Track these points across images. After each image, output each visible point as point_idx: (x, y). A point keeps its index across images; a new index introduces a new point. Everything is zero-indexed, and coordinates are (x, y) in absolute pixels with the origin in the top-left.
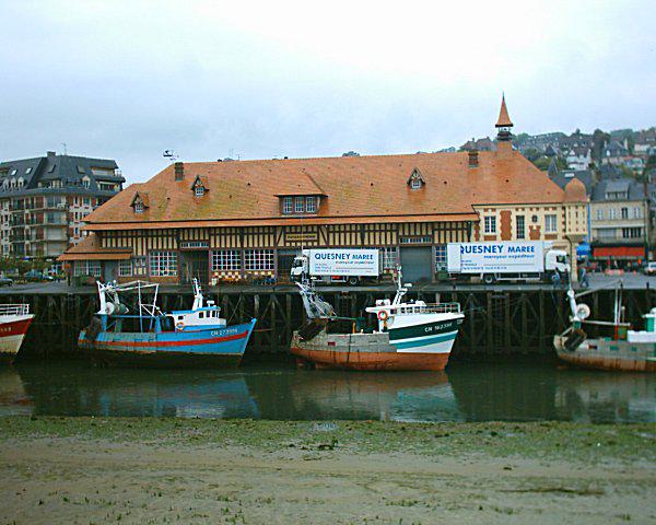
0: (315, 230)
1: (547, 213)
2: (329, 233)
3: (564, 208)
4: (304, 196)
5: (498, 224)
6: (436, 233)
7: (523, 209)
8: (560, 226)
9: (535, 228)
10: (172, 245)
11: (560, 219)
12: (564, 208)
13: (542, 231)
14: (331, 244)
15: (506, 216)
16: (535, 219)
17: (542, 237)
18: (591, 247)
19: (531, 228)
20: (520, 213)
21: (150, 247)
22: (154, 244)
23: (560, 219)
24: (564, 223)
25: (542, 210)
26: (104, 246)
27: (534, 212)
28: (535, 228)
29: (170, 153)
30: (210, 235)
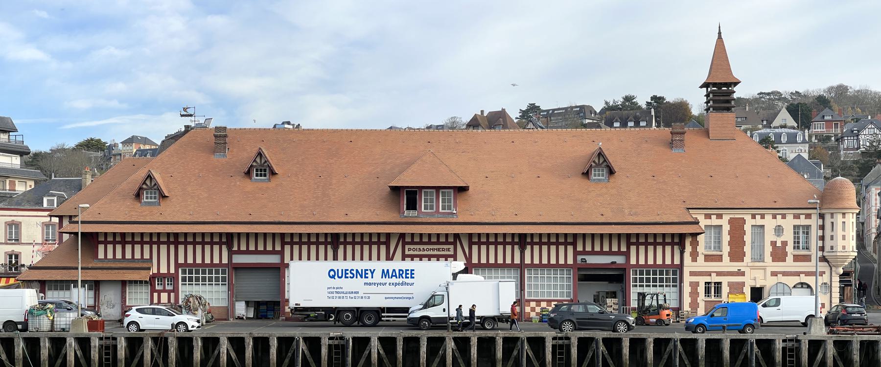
0: (451, 240)
1: (797, 222)
2: (471, 244)
3: (822, 216)
4: (438, 188)
5: (726, 238)
6: (633, 249)
7: (763, 217)
8: (814, 243)
9: (779, 244)
10: (219, 255)
11: (815, 233)
12: (822, 216)
13: (790, 249)
14: (484, 261)
15: (737, 227)
16: (779, 230)
17: (790, 258)
19: (773, 244)
20: (759, 221)
21: (181, 260)
23: (815, 233)
24: (822, 238)
25: (768, 218)
26: (101, 255)
27: (779, 220)
28: (779, 244)
29: (190, 112)
30: (283, 244)
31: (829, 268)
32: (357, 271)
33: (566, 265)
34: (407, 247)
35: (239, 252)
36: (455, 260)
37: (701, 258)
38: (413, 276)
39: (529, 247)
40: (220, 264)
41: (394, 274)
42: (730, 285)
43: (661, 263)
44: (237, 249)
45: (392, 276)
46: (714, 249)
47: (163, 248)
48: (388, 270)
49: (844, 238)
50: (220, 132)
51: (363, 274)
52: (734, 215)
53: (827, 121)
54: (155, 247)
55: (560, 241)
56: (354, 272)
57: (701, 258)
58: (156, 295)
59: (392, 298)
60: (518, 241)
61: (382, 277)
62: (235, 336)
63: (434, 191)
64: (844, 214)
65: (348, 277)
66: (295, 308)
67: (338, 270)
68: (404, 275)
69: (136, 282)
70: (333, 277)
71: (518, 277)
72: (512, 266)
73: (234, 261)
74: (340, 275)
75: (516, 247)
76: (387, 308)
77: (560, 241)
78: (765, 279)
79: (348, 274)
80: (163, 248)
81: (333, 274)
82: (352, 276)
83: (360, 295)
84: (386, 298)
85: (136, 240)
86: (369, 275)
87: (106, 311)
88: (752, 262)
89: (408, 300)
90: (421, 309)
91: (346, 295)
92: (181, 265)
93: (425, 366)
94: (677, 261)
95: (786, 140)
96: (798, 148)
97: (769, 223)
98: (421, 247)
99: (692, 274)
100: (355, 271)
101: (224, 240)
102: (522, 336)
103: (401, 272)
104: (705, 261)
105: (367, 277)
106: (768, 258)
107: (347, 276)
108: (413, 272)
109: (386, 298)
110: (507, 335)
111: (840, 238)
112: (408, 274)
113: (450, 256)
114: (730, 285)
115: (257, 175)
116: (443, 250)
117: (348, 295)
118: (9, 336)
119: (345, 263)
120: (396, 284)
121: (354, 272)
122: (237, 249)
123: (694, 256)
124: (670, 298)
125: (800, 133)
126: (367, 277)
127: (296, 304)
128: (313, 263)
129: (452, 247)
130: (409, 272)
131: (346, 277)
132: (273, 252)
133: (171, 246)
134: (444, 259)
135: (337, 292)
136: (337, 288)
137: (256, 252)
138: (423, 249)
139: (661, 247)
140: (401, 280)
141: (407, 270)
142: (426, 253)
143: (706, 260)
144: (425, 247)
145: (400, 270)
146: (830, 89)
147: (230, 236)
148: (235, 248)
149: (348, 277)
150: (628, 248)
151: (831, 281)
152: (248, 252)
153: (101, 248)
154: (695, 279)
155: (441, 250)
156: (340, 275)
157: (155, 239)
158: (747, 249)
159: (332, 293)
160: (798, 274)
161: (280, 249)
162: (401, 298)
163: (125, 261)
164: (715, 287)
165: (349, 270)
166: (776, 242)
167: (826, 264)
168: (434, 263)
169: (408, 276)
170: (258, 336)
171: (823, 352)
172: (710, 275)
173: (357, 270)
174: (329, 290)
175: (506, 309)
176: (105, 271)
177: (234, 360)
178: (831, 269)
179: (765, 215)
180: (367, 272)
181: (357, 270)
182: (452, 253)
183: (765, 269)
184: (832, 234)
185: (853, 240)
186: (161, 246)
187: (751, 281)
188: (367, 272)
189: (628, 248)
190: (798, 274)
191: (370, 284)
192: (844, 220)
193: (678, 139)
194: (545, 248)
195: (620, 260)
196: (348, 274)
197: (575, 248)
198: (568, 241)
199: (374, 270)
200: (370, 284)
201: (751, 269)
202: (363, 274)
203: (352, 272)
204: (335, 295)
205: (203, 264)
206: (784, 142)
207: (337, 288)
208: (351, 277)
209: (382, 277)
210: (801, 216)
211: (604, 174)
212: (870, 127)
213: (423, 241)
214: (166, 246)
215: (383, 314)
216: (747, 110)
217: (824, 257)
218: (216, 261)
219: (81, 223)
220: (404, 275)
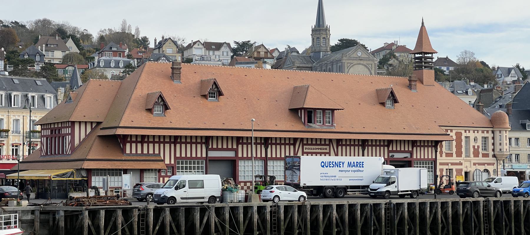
0: (327, 143)
10: (200, 151)
11: (491, 141)
13: (480, 150)
15: (459, 135)
16: (475, 139)
17: (481, 155)
18: (277, 59)
19: (474, 147)
20: (468, 134)
21: (178, 155)
22: (183, 151)
23: (491, 141)
24: (493, 144)
25: (471, 132)
26: (128, 151)
27: (476, 134)
31: (496, 161)
32: (335, 163)
34: (305, 147)
35: (213, 149)
36: (330, 155)
37: (444, 155)
38: (363, 166)
39: (270, 146)
40: (201, 158)
41: (354, 165)
42: (457, 170)
43: (423, 158)
44: (211, 147)
45: (353, 166)
46: (448, 149)
47: (167, 146)
48: (351, 162)
50: (177, 66)
51: (338, 165)
52: (457, 130)
53: (113, 51)
54: (162, 145)
55: (182, 141)
56: (334, 163)
57: (444, 155)
58: (161, 179)
59: (352, 180)
60: (204, 141)
61: (348, 167)
62: (340, 204)
63: (331, 111)
64: (506, 131)
65: (330, 167)
66: (303, 186)
67: (326, 162)
68: (359, 165)
69: (149, 170)
70: (323, 167)
71: (262, 166)
73: (209, 155)
74: (327, 166)
75: (360, 147)
76: (350, 186)
77: (182, 141)
78: (471, 167)
79: (331, 164)
80: (167, 146)
81: (323, 165)
82: (333, 166)
83: (336, 178)
84: (350, 180)
85: (166, 140)
86: (341, 166)
88: (465, 157)
89: (360, 181)
90: (386, 186)
91: (329, 178)
92: (178, 158)
93: (136, 232)
94: (434, 157)
95: (114, 65)
96: (111, 72)
97: (472, 135)
98: (312, 147)
99: (441, 164)
100: (334, 162)
101: (204, 141)
102: (471, 201)
103: (357, 164)
104: (446, 157)
105: (340, 167)
106: (472, 155)
107: (330, 166)
108: (363, 163)
109: (350, 180)
110: (464, 200)
112: (361, 165)
113: (327, 153)
114: (457, 170)
115: (210, 97)
116: (323, 149)
117: (331, 178)
118: (223, 205)
120: (355, 171)
121: (334, 163)
122: (211, 147)
123: (441, 153)
124: (430, 178)
125: (132, 61)
126: (340, 167)
127: (304, 184)
128: (378, 158)
129: (328, 147)
130: (361, 163)
131: (330, 167)
132: (232, 150)
134: (306, 154)
135: (325, 176)
136: (325, 174)
137: (222, 149)
138: (313, 148)
139: (190, 145)
140: (357, 169)
141: (360, 162)
142: (314, 151)
143: (483, 157)
144: (314, 147)
145: (357, 162)
146: (37, 23)
147: (208, 138)
148: (210, 147)
149: (330, 167)
150: (237, 146)
151: (497, 168)
152: (217, 149)
153: (128, 145)
154: (442, 167)
155: (322, 149)
156: (327, 166)
157: (162, 140)
158: (463, 150)
159: (323, 177)
160: (484, 164)
162: (357, 180)
163: (143, 155)
164: (449, 172)
165: (331, 162)
166: (475, 146)
167: (495, 159)
168: (314, 156)
169: (360, 166)
170: (352, 203)
171: (77, 222)
172: (448, 165)
173: (335, 162)
174: (321, 175)
175: (424, 186)
176: (135, 162)
177: (337, 219)
178: (497, 162)
179: (479, 131)
180: (340, 163)
181: (335, 162)
182: (328, 151)
183: (470, 162)
184: (500, 142)
186: (133, 144)
187: (465, 168)
188: (340, 163)
189: (237, 146)
190: (484, 164)
191: (342, 171)
192: (500, 134)
193: (414, 84)
194: (183, 146)
196: (331, 164)
197: (388, 149)
198: (138, 140)
199: (344, 162)
200: (342, 171)
201: (465, 161)
202: (338, 165)
203: (333, 163)
204: (324, 178)
205: (186, 158)
206: (122, 67)
207: (325, 174)
208: (332, 167)
209: (348, 167)
210: (467, 131)
211: (215, 96)
212: (162, 59)
213: (161, 141)
214: (190, 145)
215: (348, 190)
216: (57, 39)
217: (494, 155)
218: (199, 155)
220: (359, 165)
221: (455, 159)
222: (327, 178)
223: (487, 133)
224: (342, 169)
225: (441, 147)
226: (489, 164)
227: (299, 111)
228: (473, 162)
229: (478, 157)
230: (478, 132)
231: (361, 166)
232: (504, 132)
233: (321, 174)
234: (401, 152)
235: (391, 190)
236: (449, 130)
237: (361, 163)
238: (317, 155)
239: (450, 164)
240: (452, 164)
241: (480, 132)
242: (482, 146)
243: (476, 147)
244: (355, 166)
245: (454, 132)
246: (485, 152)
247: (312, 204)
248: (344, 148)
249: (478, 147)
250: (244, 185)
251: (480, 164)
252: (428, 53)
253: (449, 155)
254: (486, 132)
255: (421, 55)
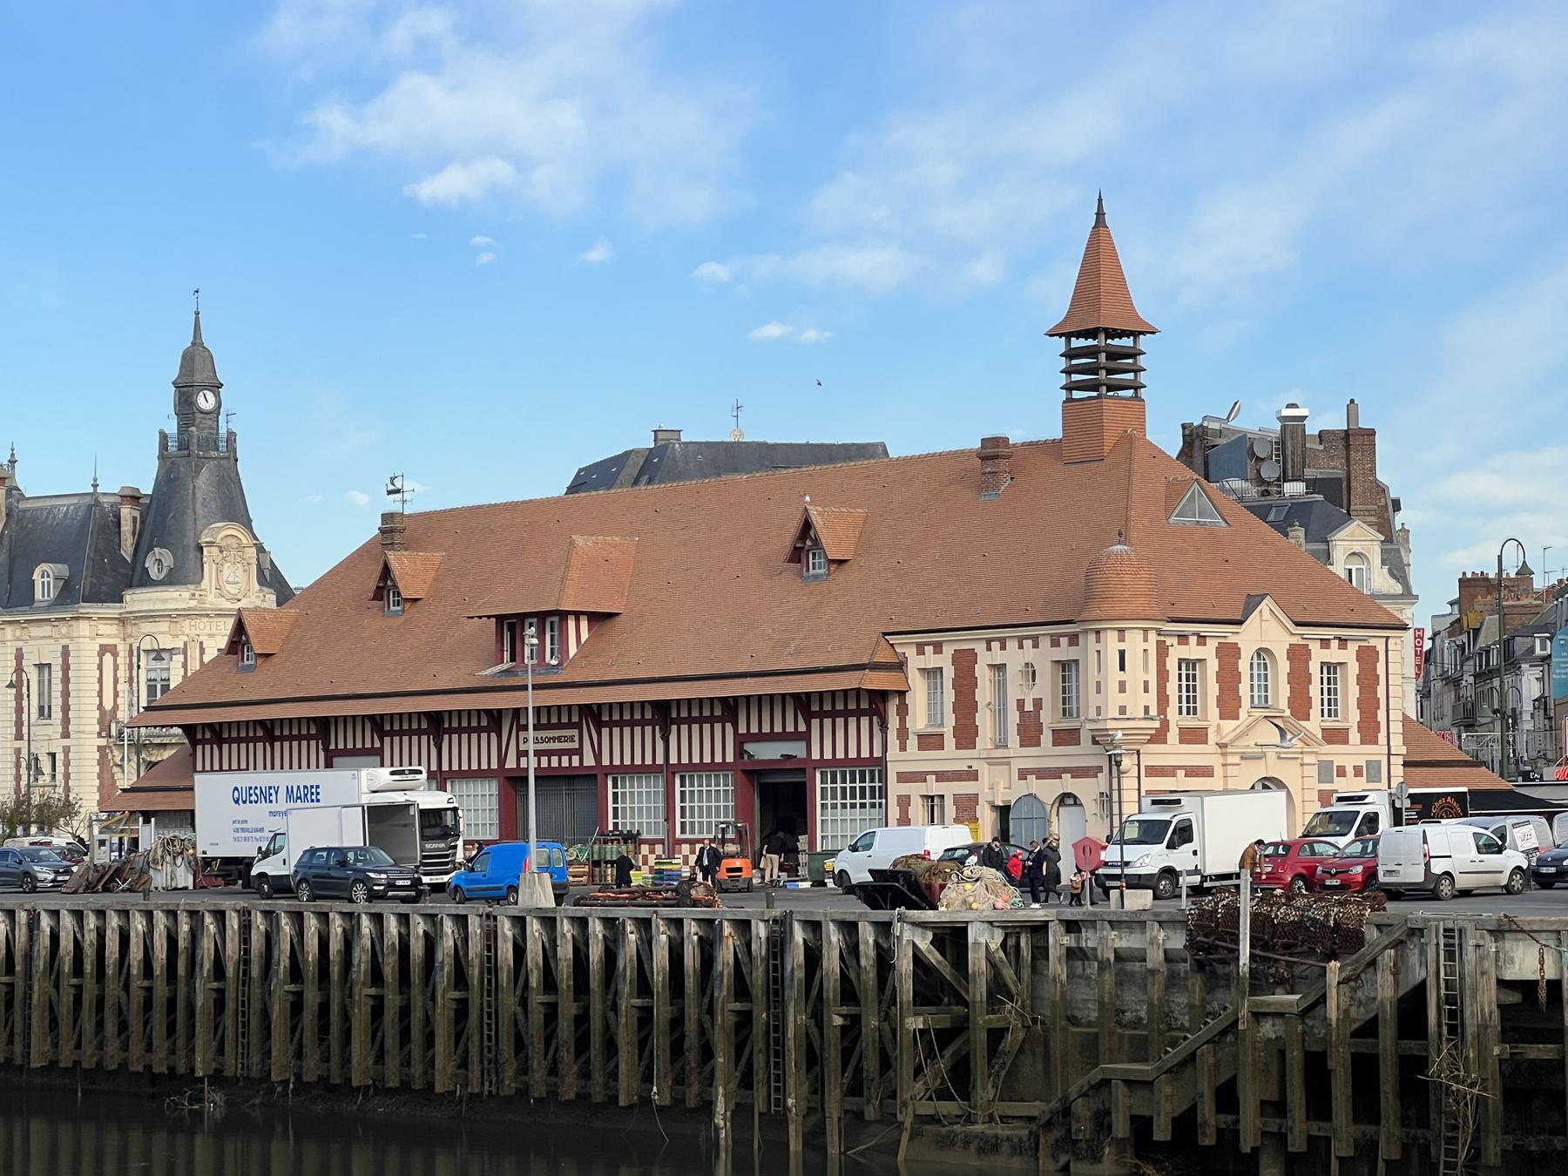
13: (1046, 717)
15: (964, 662)
17: (1047, 737)
20: (998, 656)
21: (434, 768)
25: (1012, 645)
33: (724, 766)
37: (912, 742)
45: (298, 798)
49: (1122, 687)
56: (258, 792)
57: (912, 742)
64: (1098, 632)
72: (653, 769)
87: (922, 866)
97: (1014, 657)
99: (903, 777)
106: (1014, 738)
111: (1113, 687)
114: (958, 799)
117: (253, 834)
119: (291, 775)
123: (903, 734)
129: (575, 732)
130: (314, 790)
131: (251, 802)
133: (682, 726)
150: (809, 726)
154: (905, 789)
160: (1056, 773)
161: (804, 730)
182: (576, 745)
183: (1009, 764)
185: (1146, 690)
190: (1056, 773)
195: (796, 749)
197: (736, 728)
219: (533, 689)
220: (309, 796)
221: (951, 757)
222: (247, 835)
223: (934, 653)
224: (273, 807)
225: (903, 711)
226: (1078, 773)
227: (571, 624)
228: (1017, 765)
229: (1038, 744)
230: (1036, 646)
231: (314, 797)
232: (1092, 637)
233: (234, 822)
234: (772, 737)
235: (271, 871)
236: (928, 644)
237: (314, 790)
238: (335, 760)
239: (1181, 773)
240: (941, 777)
241: (1045, 643)
242: (1180, 697)
243: (1029, 707)
244: (300, 798)
245: (948, 650)
246: (1191, 722)
247: (860, 923)
248: (852, 721)
249: (1038, 703)
250: (650, 853)
251: (1042, 774)
252: (1126, 333)
253: (930, 741)
254: (932, 647)
255: (1090, 342)
